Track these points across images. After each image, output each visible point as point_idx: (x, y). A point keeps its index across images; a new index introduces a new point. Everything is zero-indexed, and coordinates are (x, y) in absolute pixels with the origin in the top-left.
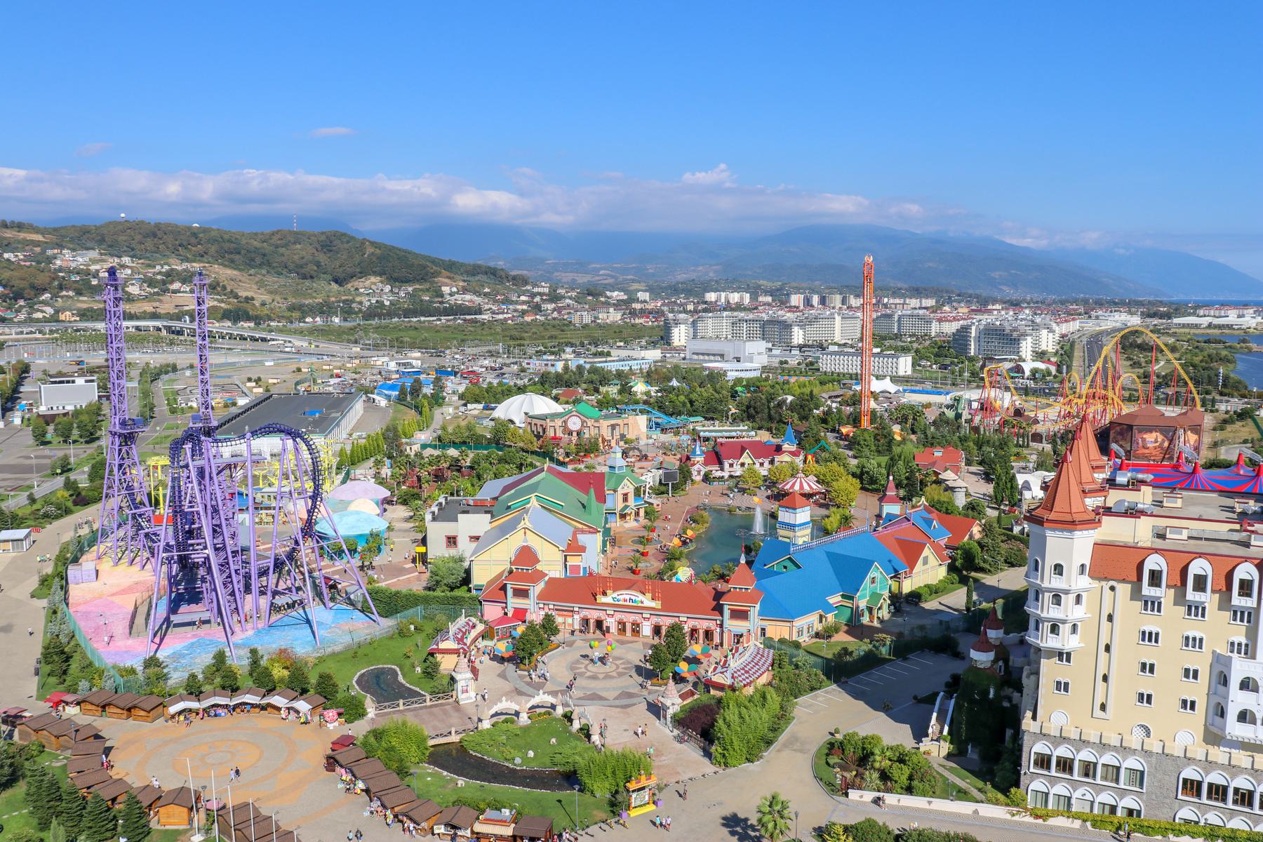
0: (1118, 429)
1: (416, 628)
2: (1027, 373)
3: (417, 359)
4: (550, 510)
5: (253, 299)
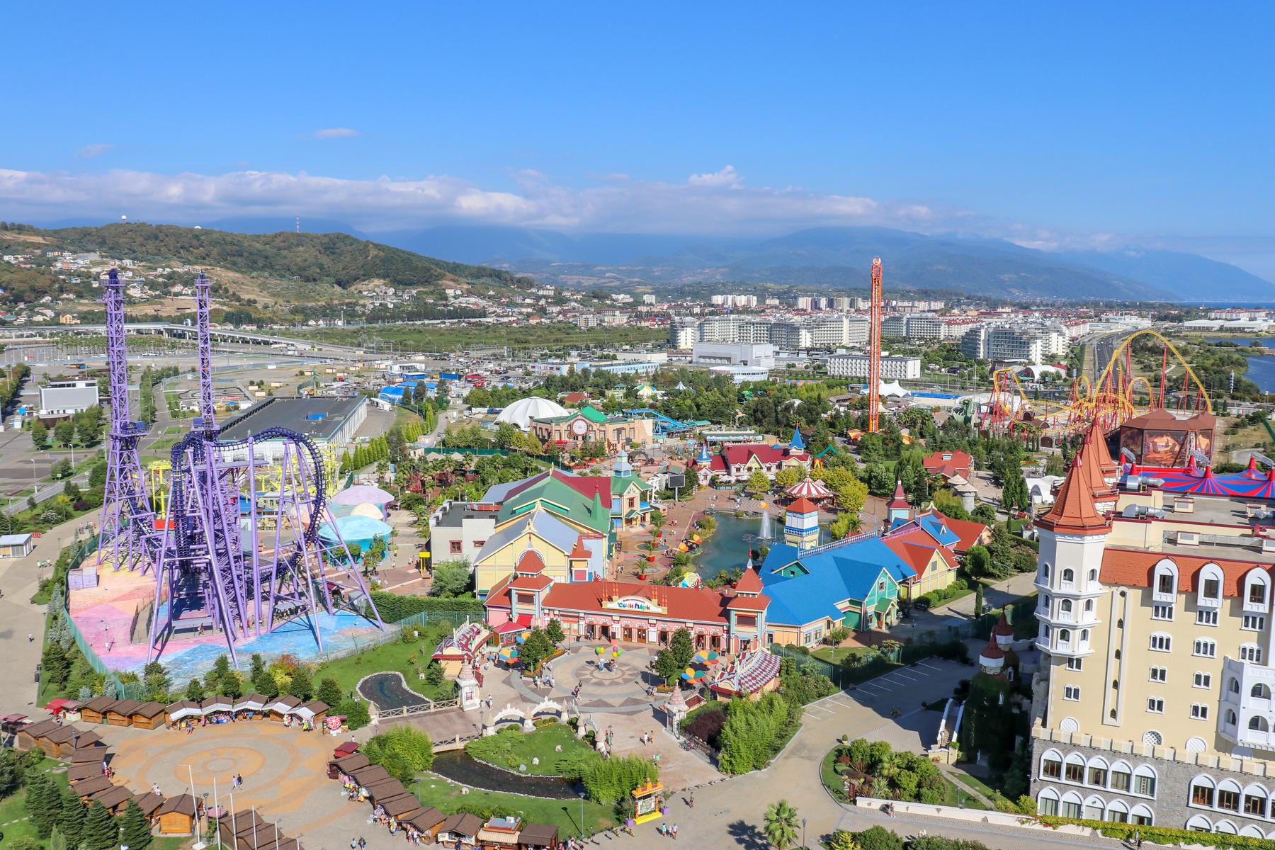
0: (1129, 433)
1: (420, 634)
2: (1037, 377)
3: (421, 362)
4: (555, 515)
5: (255, 302)
